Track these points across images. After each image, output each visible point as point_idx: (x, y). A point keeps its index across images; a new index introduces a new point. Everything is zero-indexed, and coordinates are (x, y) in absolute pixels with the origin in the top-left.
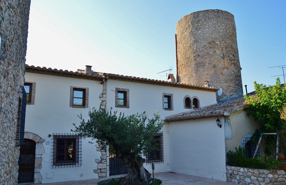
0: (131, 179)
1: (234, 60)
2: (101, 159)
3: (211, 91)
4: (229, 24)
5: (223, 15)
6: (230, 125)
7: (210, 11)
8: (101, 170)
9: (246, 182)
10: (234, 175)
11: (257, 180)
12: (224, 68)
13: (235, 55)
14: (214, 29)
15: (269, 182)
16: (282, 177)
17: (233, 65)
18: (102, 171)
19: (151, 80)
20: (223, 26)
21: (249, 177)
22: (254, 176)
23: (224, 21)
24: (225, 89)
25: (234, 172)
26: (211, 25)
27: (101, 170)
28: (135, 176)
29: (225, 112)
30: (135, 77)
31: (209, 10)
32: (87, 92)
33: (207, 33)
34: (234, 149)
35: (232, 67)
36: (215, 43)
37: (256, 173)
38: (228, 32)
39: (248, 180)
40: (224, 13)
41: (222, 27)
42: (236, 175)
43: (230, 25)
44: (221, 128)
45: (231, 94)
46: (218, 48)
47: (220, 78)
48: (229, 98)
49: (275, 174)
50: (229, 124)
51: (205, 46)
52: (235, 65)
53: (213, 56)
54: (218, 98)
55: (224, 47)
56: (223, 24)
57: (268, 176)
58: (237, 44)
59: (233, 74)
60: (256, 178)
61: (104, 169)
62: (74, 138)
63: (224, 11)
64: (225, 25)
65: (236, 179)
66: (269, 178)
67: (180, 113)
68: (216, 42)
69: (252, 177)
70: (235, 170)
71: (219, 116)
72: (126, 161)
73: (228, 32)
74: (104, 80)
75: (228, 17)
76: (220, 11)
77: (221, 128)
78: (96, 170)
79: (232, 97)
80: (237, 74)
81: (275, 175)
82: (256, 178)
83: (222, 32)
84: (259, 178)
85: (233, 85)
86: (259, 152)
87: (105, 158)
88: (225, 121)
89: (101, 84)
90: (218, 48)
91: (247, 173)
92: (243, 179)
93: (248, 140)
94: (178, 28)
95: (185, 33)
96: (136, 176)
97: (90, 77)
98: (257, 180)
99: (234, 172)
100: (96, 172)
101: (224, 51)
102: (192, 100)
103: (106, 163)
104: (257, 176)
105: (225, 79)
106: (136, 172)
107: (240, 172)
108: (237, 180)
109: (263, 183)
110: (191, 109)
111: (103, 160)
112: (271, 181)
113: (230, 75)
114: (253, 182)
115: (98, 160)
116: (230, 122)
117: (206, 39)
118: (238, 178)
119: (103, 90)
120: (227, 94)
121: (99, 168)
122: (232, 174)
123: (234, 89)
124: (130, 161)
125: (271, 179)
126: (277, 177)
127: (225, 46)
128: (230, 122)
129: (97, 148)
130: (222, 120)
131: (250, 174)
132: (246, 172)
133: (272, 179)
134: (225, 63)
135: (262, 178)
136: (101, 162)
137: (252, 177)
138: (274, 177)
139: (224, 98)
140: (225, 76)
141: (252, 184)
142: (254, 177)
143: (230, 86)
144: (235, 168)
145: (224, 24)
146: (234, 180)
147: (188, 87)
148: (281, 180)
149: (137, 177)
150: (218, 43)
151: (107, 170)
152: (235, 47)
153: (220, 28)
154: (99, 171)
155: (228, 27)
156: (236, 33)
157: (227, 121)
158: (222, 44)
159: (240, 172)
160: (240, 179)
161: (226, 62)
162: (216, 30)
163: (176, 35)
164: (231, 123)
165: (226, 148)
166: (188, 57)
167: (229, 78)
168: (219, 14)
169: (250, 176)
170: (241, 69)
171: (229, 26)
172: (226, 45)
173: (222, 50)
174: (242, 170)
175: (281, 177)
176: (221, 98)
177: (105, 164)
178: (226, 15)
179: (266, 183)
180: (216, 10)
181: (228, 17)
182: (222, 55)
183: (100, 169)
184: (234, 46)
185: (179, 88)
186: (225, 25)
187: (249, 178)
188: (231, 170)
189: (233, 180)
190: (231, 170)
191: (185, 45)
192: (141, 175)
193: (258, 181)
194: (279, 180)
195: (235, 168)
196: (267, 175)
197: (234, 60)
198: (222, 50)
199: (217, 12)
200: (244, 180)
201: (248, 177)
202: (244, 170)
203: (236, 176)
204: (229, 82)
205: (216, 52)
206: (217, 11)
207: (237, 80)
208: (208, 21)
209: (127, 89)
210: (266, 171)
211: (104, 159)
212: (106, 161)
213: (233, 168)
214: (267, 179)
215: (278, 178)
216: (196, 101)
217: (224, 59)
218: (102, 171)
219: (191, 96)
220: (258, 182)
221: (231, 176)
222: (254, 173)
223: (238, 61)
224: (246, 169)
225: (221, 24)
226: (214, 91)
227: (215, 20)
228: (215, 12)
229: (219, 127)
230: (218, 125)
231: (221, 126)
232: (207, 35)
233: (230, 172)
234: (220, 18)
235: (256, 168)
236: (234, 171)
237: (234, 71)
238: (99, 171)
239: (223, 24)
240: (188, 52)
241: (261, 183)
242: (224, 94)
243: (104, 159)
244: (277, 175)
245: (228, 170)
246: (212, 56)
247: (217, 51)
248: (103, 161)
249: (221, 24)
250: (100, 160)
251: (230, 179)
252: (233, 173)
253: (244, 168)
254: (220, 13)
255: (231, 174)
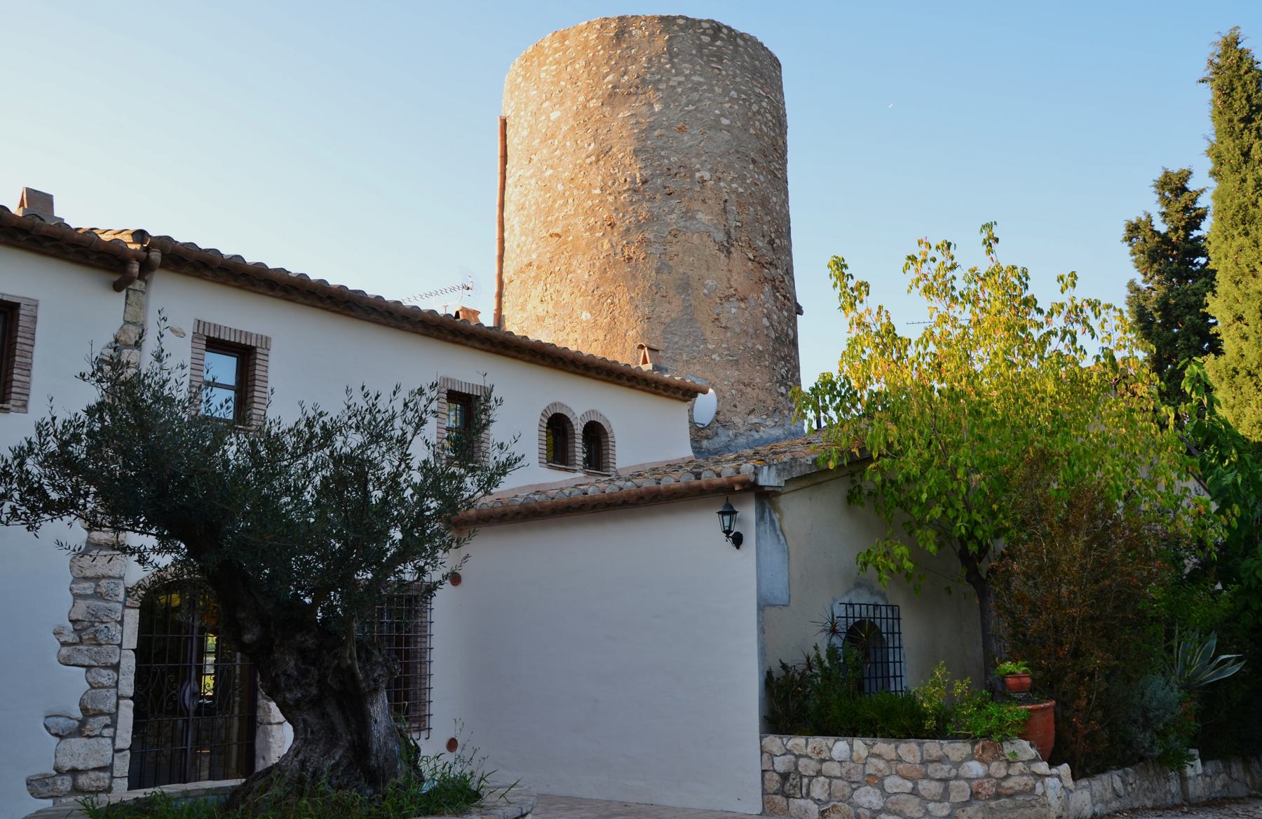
0: (314, 773)
1: (771, 264)
2: (84, 709)
3: (669, 397)
4: (758, 95)
5: (736, 51)
6: (781, 537)
7: (681, 22)
8: (74, 780)
9: (859, 807)
10: (802, 777)
11: (914, 792)
12: (728, 298)
13: (777, 241)
14: (691, 107)
15: (967, 798)
16: (1022, 774)
17: (767, 288)
18: (83, 780)
19: (387, 302)
20: (732, 100)
21: (876, 781)
22: (897, 773)
23: (738, 79)
24: (727, 395)
25: (802, 762)
26: (679, 90)
27: (74, 780)
28: (338, 754)
29: (766, 468)
30: (303, 278)
31: (675, 18)
32: (23, 321)
33: (660, 126)
34: (813, 648)
35: (762, 297)
36: (692, 176)
37: (909, 758)
38: (752, 131)
39: (868, 798)
40: (740, 42)
41: (727, 105)
42: (811, 778)
43: (764, 104)
44: (738, 548)
45: (753, 419)
46: (704, 201)
47: (705, 341)
48: (742, 440)
49: (994, 759)
50: (779, 532)
52: (775, 288)
53: (681, 237)
54: (698, 433)
55: (734, 197)
57: (962, 772)
58: (786, 194)
59: (767, 327)
60: (910, 785)
61: (94, 769)
63: (742, 35)
64: (743, 96)
65: (813, 799)
66: (968, 780)
67: (519, 488)
69: (892, 783)
70: (807, 756)
71: (737, 488)
72: (290, 664)
73: (752, 131)
74: (135, 268)
75: (757, 63)
76: (725, 31)
77: (738, 548)
78: (43, 779)
79: (757, 436)
80: (783, 329)
81: (994, 764)
82: (910, 785)
83: (729, 128)
84: (924, 785)
85: (767, 378)
86: (901, 676)
87: (109, 705)
88: (761, 518)
89: (117, 287)
90: (704, 201)
91: (864, 764)
92: (844, 796)
93: (857, 615)
94: (518, 86)
95: (555, 115)
96: (340, 752)
97: (53, 239)
98: (914, 792)
99: (802, 762)
100: (44, 790)
101: (731, 217)
102: (579, 429)
103: (113, 739)
104: (914, 774)
105: (728, 349)
106: (340, 730)
107: (831, 760)
108: (817, 801)
109: (940, 805)
110: (575, 471)
111: (95, 715)
112: (975, 795)
113: (751, 331)
114: (896, 807)
115: (61, 720)
118: (818, 790)
119: (127, 322)
120: (737, 420)
121: (67, 764)
122: (792, 776)
123: (769, 402)
124: (312, 669)
125: (975, 783)
126: (1003, 773)
127: (740, 195)
128: (780, 520)
129: (64, 644)
130: (748, 512)
131: (881, 764)
132: (860, 758)
133: (981, 785)
134: (735, 276)
135: (937, 784)
136: (79, 732)
137: (887, 782)
138: (988, 776)
139: (723, 437)
140: (729, 334)
141: (889, 812)
142: (898, 780)
143: (749, 385)
144: (807, 745)
145: (739, 91)
146: (802, 802)
147: (565, 363)
148: (1017, 788)
149: (345, 762)
150: (707, 176)
151: (112, 777)
152: (778, 208)
153: (721, 109)
154: (65, 783)
155: (755, 108)
156: (785, 144)
157: (767, 514)
158: (722, 184)
159: (831, 760)
160: (830, 795)
161: (738, 272)
163: (504, 124)
164: (786, 528)
165: (763, 653)
166: (558, 230)
167: (750, 345)
168: (719, 43)
169: (882, 780)
170: (799, 311)
171: (760, 107)
172: (741, 190)
173: (725, 210)
174: (840, 747)
175: (1017, 772)
176: (707, 438)
177: (103, 741)
178: (749, 55)
179: (956, 806)
180: (708, 21)
181: (757, 63)
182: (720, 237)
183: (74, 772)
184: (774, 199)
185: (519, 362)
186: (743, 96)
187: (875, 786)
188: (788, 752)
189: (797, 803)
190: (788, 752)
191: (550, 172)
192: (375, 747)
193: (918, 800)
194: (1011, 788)
195: (807, 745)
196: (957, 765)
197: (771, 264)
198: (725, 210)
199: (710, 32)
200: (848, 800)
201: (868, 783)
202: (852, 750)
203: (810, 782)
204: (747, 366)
205: (693, 218)
206: (712, 28)
207: (783, 358)
208: (669, 71)
209: (261, 333)
210: (958, 749)
211: (101, 713)
212: (114, 725)
213: (797, 742)
214: (957, 787)
215: (1008, 776)
216: (596, 434)
217: (729, 253)
218: (83, 780)
219: (574, 409)
220: (920, 805)
221: (783, 785)
222: (899, 760)
223: (789, 271)
224: (859, 744)
225: (726, 92)
226: (679, 396)
227: (698, 67)
229: (729, 545)
230: (727, 532)
231: (738, 540)
232: (656, 133)
233: (781, 764)
234: (720, 60)
235: (908, 736)
236: (798, 757)
237: (769, 317)
238: (65, 783)
240: (561, 206)
241: (931, 806)
242: (721, 418)
243: (101, 713)
244: (1003, 765)
245: (772, 755)
246: (675, 236)
247: (700, 216)
248: (96, 724)
250: (79, 715)
251: (778, 798)
252: (796, 769)
253: (850, 739)
254: (722, 39)
255: (785, 777)
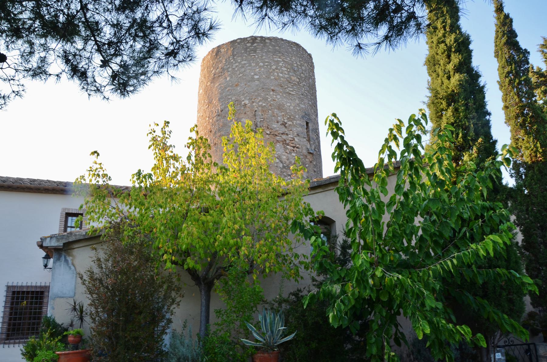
7: (238, 41)
14: (241, 75)
20: (260, 67)
36: (241, 104)
40: (267, 41)
41: (257, 70)
51: (222, 111)
56: (261, 64)
62: (11, 294)
68: (243, 101)
73: (272, 77)
83: (258, 80)
116: (72, 260)
117: (226, 97)
150: (247, 102)
155: (274, 67)
158: (254, 104)
162: (244, 77)
168: (255, 45)
173: (255, 115)
198: (255, 115)
208: (232, 62)
227: (244, 58)
228: (247, 43)
237: (279, 158)
239: (261, 64)
249: (257, 64)
